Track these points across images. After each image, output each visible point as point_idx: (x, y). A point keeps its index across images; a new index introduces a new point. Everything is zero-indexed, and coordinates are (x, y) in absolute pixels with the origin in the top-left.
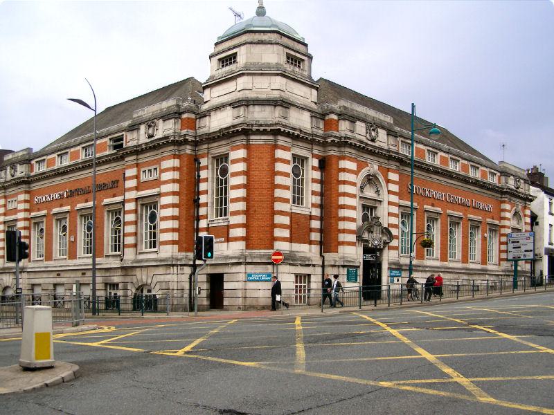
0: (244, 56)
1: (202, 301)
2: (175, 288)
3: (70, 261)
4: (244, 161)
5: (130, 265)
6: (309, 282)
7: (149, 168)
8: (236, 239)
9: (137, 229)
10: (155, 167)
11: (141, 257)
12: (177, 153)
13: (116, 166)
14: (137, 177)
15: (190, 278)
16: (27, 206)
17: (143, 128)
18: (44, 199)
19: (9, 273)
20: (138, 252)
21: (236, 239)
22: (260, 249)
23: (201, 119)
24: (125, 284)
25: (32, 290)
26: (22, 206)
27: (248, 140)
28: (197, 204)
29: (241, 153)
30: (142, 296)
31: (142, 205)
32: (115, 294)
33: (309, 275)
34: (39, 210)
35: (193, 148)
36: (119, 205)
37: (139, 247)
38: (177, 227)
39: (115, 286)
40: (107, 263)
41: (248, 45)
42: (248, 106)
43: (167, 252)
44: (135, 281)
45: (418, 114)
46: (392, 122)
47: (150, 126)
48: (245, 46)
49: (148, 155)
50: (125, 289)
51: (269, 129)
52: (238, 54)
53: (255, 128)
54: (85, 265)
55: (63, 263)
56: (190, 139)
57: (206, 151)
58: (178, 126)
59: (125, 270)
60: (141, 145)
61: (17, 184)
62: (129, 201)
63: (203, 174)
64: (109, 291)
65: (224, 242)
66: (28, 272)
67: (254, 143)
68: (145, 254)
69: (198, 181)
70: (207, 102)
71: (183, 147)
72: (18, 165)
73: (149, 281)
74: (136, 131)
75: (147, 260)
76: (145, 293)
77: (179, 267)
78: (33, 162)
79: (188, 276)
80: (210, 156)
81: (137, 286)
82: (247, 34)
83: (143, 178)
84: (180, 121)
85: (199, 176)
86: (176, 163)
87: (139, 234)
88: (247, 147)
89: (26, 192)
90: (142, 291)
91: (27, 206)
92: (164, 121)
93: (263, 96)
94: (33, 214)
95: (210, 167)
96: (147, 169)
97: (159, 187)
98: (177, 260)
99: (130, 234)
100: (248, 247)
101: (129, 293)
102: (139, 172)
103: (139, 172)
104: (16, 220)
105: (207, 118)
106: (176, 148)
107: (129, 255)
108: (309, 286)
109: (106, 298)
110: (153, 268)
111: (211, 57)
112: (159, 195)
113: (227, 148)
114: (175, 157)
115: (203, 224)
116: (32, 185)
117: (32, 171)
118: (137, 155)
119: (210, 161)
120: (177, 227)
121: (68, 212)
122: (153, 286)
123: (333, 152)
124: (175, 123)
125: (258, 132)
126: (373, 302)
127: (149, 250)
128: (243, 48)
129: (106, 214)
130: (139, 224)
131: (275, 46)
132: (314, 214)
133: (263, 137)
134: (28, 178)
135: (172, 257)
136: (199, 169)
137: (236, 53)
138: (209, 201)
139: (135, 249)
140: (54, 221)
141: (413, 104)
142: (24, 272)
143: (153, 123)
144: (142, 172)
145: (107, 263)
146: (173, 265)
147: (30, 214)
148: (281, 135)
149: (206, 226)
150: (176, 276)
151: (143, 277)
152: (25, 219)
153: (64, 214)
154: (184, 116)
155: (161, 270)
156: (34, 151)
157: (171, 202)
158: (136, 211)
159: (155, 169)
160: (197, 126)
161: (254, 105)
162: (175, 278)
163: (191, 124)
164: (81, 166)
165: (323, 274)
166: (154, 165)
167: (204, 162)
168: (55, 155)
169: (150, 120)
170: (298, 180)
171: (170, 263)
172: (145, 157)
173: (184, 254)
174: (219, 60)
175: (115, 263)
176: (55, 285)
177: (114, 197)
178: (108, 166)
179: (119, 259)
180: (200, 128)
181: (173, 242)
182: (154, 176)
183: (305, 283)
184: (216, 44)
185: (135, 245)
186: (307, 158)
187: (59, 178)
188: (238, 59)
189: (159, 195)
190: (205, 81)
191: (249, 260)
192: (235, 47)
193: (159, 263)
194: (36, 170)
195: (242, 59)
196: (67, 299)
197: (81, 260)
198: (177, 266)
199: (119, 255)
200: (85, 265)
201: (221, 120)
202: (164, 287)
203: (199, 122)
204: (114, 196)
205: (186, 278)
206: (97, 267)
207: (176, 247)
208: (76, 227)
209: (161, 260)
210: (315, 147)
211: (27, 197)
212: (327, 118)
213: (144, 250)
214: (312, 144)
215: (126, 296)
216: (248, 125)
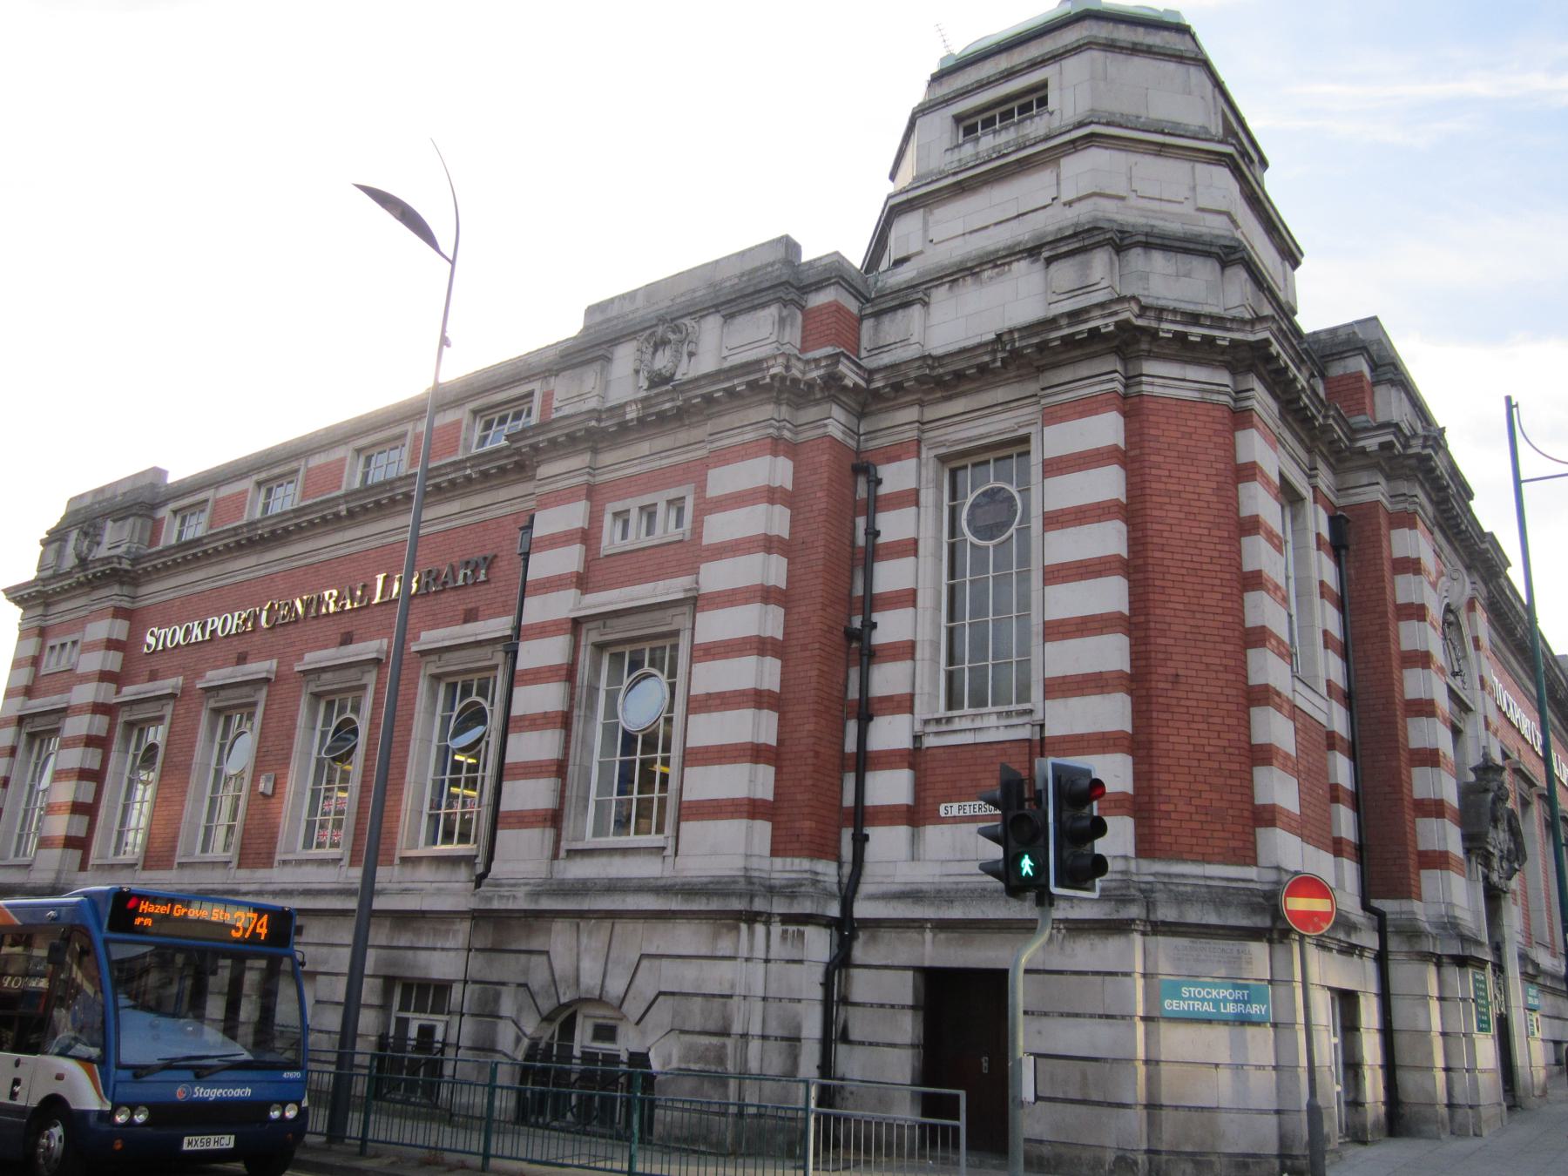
0: (1073, 90)
2: (756, 1029)
3: (244, 874)
5: (523, 904)
7: (646, 500)
10: (673, 493)
12: (787, 434)
13: (500, 502)
14: (588, 537)
15: (827, 985)
16: (114, 661)
18: (180, 636)
20: (564, 845)
22: (1205, 859)
23: (886, 319)
24: (490, 991)
26: (93, 662)
27: (1131, 380)
28: (860, 649)
30: (566, 1055)
31: (600, 647)
32: (427, 1032)
34: (153, 676)
36: (488, 650)
37: (568, 826)
38: (772, 741)
39: (432, 993)
40: (406, 891)
41: (1096, 55)
43: (725, 850)
44: (538, 979)
48: (1086, 56)
49: (645, 448)
50: (488, 1013)
51: (1224, 337)
53: (1168, 328)
54: (307, 893)
58: (793, 335)
59: (498, 927)
60: (623, 406)
61: (92, 584)
62: (544, 630)
64: (395, 1012)
67: (1157, 391)
71: (812, 413)
72: (109, 524)
73: (616, 987)
74: (597, 366)
75: (614, 887)
76: (583, 1039)
77: (777, 929)
78: (164, 513)
79: (818, 974)
81: (547, 1005)
82: (1087, 23)
83: (611, 540)
85: (872, 533)
86: (780, 472)
87: (572, 770)
88: (1131, 406)
89: (119, 613)
90: (568, 1029)
91: (114, 661)
93: (1174, 227)
94: (130, 692)
95: (927, 497)
96: (633, 504)
97: (695, 571)
98: (771, 891)
99: (531, 770)
101: (506, 1037)
102: (595, 518)
103: (595, 518)
104: (63, 712)
105: (917, 309)
106: (785, 411)
107: (522, 858)
110: (640, 926)
112: (695, 602)
114: (777, 446)
115: (890, 733)
116: (143, 590)
117: (154, 539)
118: (595, 451)
119: (929, 471)
120: (772, 741)
121: (267, 680)
122: (633, 1009)
123: (1376, 491)
124: (782, 321)
125: (1183, 349)
127: (612, 841)
128: (1070, 63)
130: (577, 727)
131: (1192, 70)
133: (1193, 372)
135: (749, 880)
136: (873, 506)
137: (1043, 85)
139: (549, 833)
140: (205, 717)
141: (1508, 399)
145: (406, 891)
146: (751, 918)
147: (118, 692)
149: (906, 743)
150: (760, 967)
151: (586, 964)
152: (98, 708)
153: (245, 690)
154: (818, 300)
155: (686, 938)
156: (171, 479)
157: (752, 631)
158: (569, 673)
160: (865, 342)
162: (751, 978)
163: (845, 329)
164: (343, 509)
166: (667, 486)
167: (895, 477)
168: (248, 484)
171: (737, 905)
172: (620, 462)
173: (805, 864)
174: (958, 119)
175: (449, 892)
177: (466, 621)
179: (463, 873)
180: (878, 349)
181: (753, 809)
182: (667, 529)
184: (937, 78)
185: (554, 819)
187: (252, 560)
188: (1053, 102)
189: (695, 602)
191: (1166, 913)
192: (1034, 65)
193: (675, 904)
197: (288, 870)
198: (767, 918)
199: (469, 860)
200: (307, 893)
202: (696, 1022)
203: (876, 329)
204: (470, 616)
205: (808, 982)
206: (379, 904)
207: (763, 829)
208: (290, 737)
209: (689, 890)
211: (120, 629)
212: (1336, 370)
213: (590, 841)
215: (486, 1046)
216: (1144, 309)
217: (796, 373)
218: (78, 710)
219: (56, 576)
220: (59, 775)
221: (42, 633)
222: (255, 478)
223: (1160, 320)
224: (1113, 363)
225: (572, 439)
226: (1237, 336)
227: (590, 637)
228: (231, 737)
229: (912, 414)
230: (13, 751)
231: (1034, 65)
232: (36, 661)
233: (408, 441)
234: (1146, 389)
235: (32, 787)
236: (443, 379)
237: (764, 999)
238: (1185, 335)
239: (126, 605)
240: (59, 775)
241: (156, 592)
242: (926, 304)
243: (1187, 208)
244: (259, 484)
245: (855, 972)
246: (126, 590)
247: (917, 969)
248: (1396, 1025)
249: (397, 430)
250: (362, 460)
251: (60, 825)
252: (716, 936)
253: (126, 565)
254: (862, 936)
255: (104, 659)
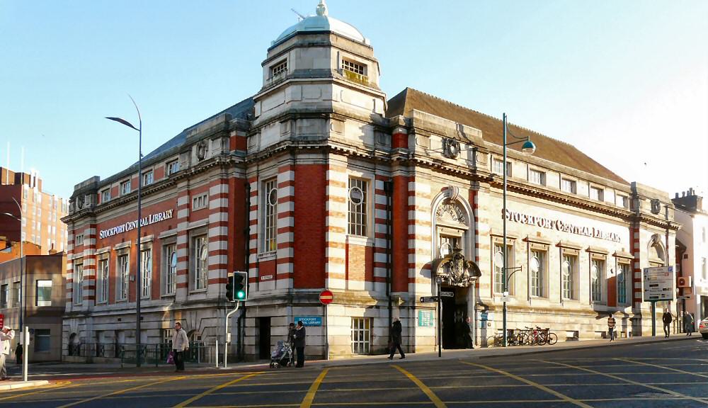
1: (251, 349)
3: (130, 303)
4: (291, 185)
6: (372, 327)
8: (283, 276)
9: (188, 266)
10: (204, 194)
11: (192, 298)
14: (189, 206)
15: (239, 323)
17: (194, 148)
19: (76, 318)
21: (283, 276)
25: (97, 337)
27: (295, 160)
29: (286, 176)
33: (372, 319)
35: (243, 171)
37: (190, 287)
42: (295, 120)
45: (510, 120)
46: (481, 136)
47: (200, 147)
52: (288, 60)
54: (117, 311)
55: (124, 306)
56: (237, 160)
57: (255, 174)
61: (83, 217)
63: (253, 201)
65: (272, 279)
66: (94, 317)
67: (301, 163)
68: (195, 295)
69: (248, 208)
70: (258, 117)
74: (188, 153)
78: (99, 192)
80: (260, 180)
84: (229, 139)
86: (224, 188)
88: (293, 168)
89: (92, 226)
92: (213, 140)
100: (296, 285)
104: (209, 226)
108: (372, 331)
109: (162, 346)
111: (263, 64)
113: (275, 170)
114: (223, 181)
124: (223, 143)
126: (271, 347)
128: (293, 52)
129: (162, 249)
130: (190, 259)
132: (377, 245)
134: (93, 210)
137: (286, 60)
138: (259, 232)
141: (504, 114)
142: (88, 317)
143: (203, 143)
144: (193, 200)
148: (302, 153)
155: (208, 314)
159: (205, 196)
161: (301, 118)
163: (241, 144)
165: (390, 317)
167: (254, 187)
168: (118, 184)
169: (200, 140)
170: (359, 207)
174: (271, 68)
176: (117, 332)
178: (163, 194)
183: (367, 327)
184: (269, 50)
186: (369, 180)
189: (209, 226)
190: (257, 93)
194: (103, 200)
195: (291, 67)
196: (149, 347)
201: (270, 137)
210: (378, 167)
211: (93, 231)
213: (196, 290)
214: (375, 164)
217: (222, 161)
218: (214, 225)
219: (75, 214)
220: (179, 260)
221: (74, 232)
222: (166, 161)
223: (298, 144)
224: (288, 157)
225: (182, 178)
226: (321, 145)
227: (191, 235)
228: (201, 247)
229: (255, 169)
230: (72, 271)
231: (280, 54)
232: (74, 242)
233: (153, 171)
234: (298, 163)
235: (169, 266)
236: (283, 93)
237: (409, 318)
238: (306, 147)
239: (94, 223)
240: (211, 254)
241: (101, 219)
242: (260, 133)
243: (320, 100)
244: (121, 183)
245: (247, 319)
246: (93, 218)
247: (256, 318)
248: (502, 314)
249: (150, 168)
250: (169, 166)
251: (86, 293)
252: (213, 313)
253: (91, 211)
254: (247, 310)
255: (221, 202)
